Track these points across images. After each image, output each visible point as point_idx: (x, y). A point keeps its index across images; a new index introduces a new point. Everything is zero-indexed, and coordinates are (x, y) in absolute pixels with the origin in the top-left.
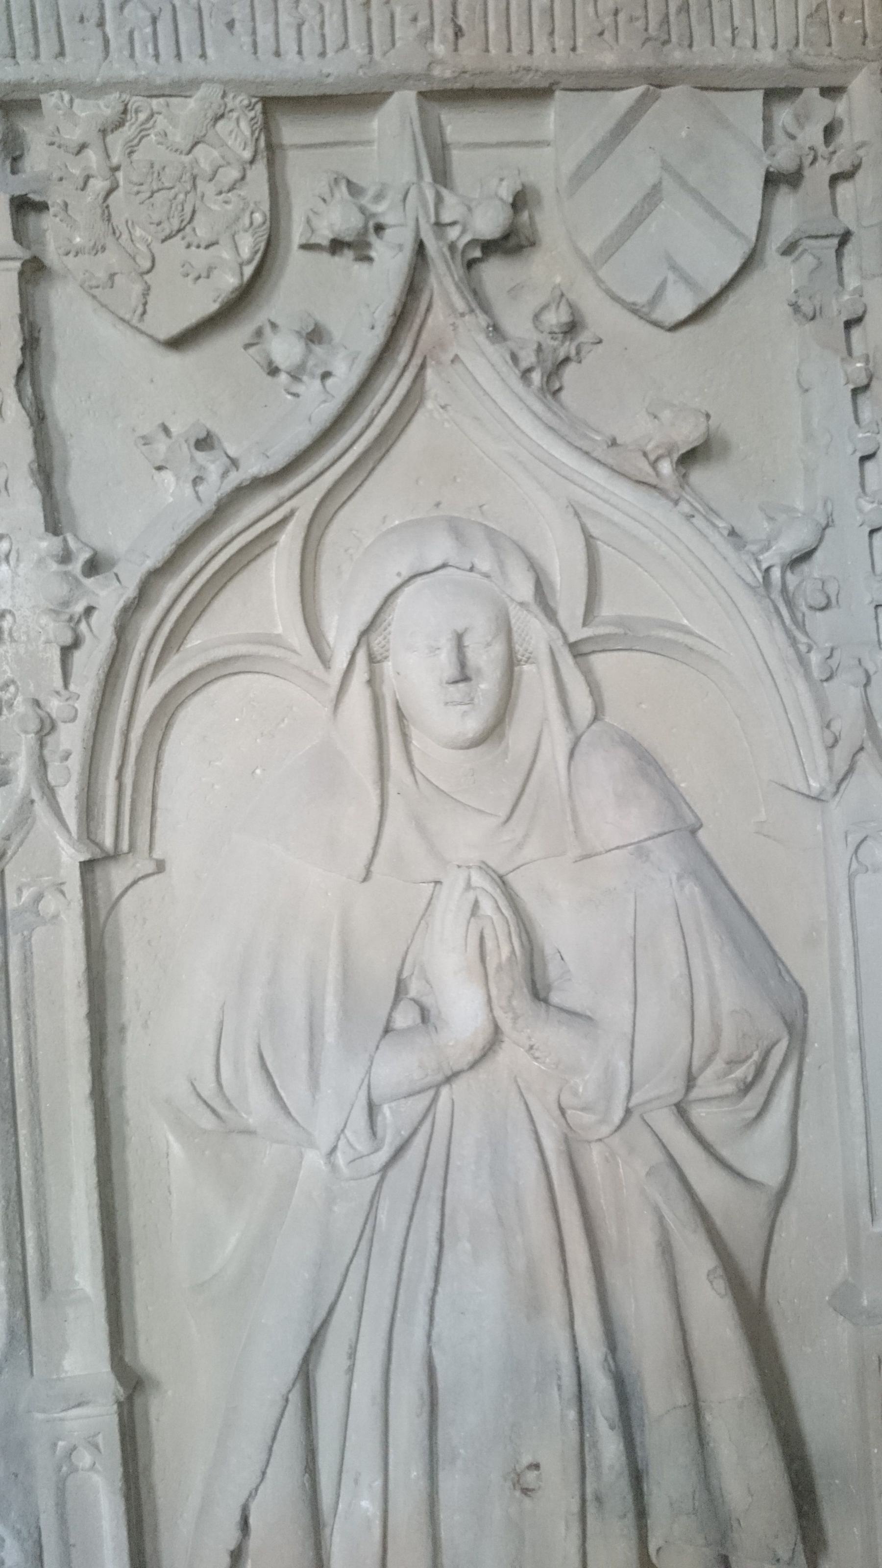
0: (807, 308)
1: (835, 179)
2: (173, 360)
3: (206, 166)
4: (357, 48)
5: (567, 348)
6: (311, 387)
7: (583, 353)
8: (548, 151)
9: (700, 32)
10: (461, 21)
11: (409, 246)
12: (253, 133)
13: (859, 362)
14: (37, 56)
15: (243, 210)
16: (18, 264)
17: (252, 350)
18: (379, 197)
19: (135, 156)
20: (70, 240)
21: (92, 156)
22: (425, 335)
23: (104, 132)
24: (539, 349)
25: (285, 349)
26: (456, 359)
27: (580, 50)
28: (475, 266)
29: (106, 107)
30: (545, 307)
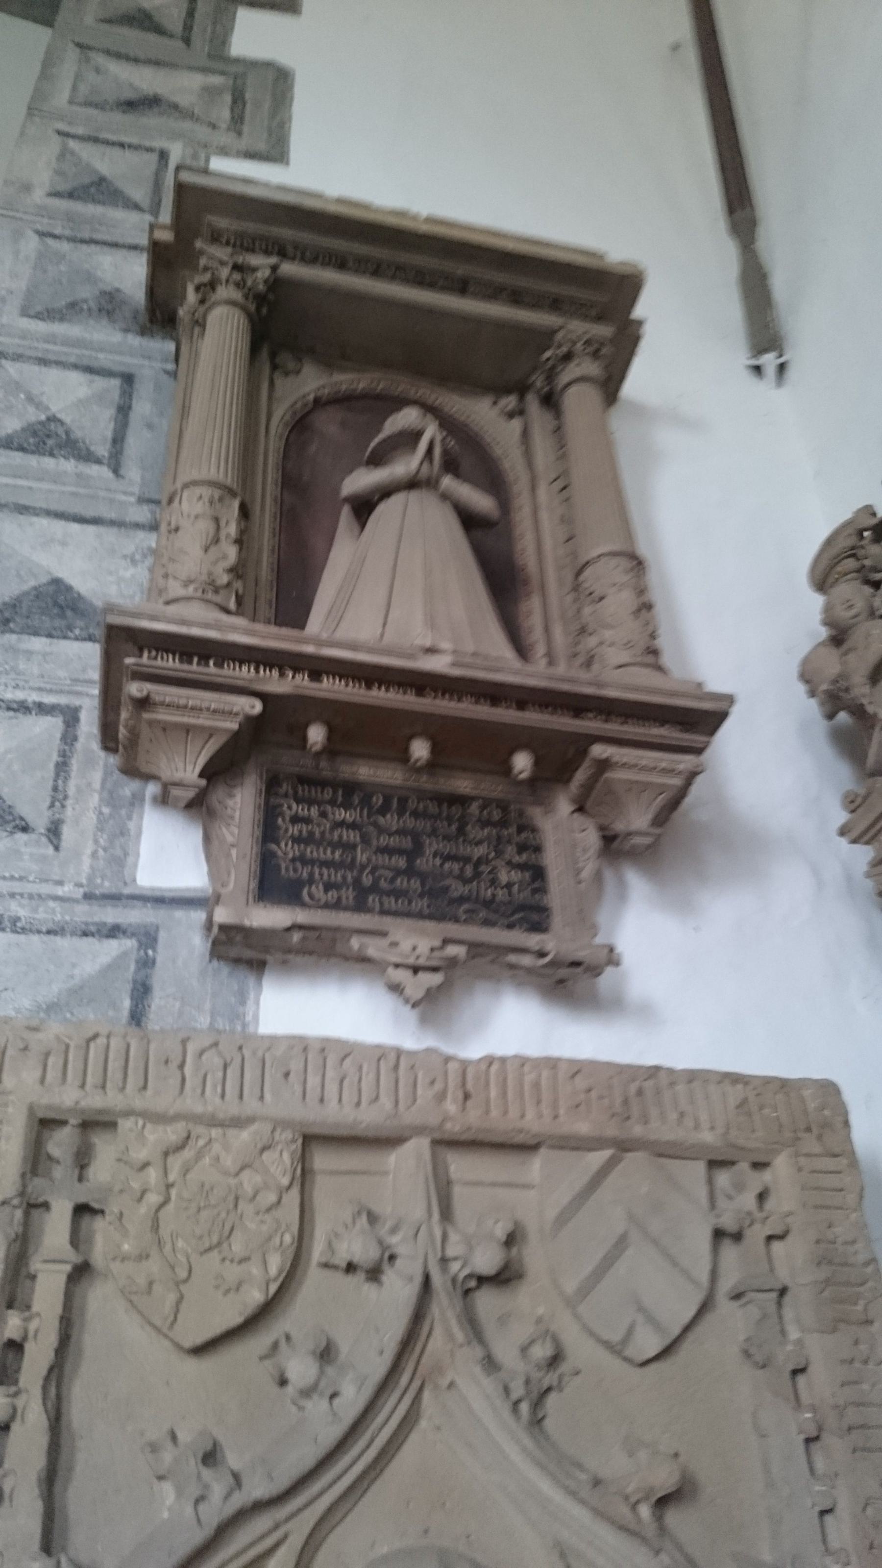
0: (759, 1358)
1: (770, 1238)
2: (192, 1365)
3: (248, 1189)
4: (386, 1102)
5: (550, 1379)
6: (318, 1406)
7: (564, 1383)
8: (532, 1193)
9: (654, 1112)
10: (470, 1086)
11: (418, 1279)
12: (292, 1163)
13: (807, 1412)
14: (123, 1089)
15: (276, 1231)
16: (68, 1268)
17: (267, 1363)
18: (394, 1230)
19: (188, 1176)
20: (119, 1247)
21: (153, 1175)
22: (424, 1360)
23: (166, 1154)
24: (527, 1382)
25: (300, 1368)
26: (451, 1385)
27: (561, 1119)
28: (471, 1295)
29: (172, 1134)
30: (532, 1342)
